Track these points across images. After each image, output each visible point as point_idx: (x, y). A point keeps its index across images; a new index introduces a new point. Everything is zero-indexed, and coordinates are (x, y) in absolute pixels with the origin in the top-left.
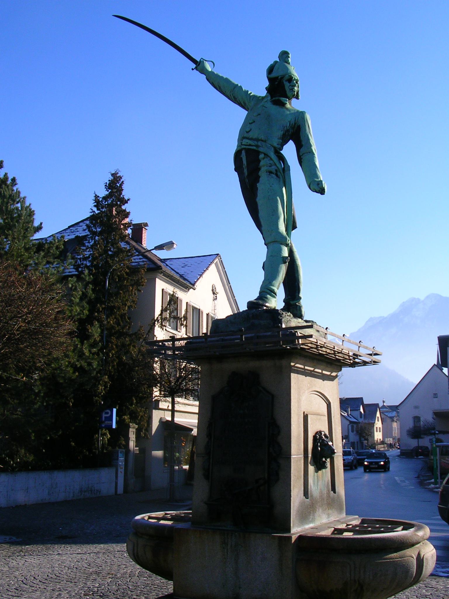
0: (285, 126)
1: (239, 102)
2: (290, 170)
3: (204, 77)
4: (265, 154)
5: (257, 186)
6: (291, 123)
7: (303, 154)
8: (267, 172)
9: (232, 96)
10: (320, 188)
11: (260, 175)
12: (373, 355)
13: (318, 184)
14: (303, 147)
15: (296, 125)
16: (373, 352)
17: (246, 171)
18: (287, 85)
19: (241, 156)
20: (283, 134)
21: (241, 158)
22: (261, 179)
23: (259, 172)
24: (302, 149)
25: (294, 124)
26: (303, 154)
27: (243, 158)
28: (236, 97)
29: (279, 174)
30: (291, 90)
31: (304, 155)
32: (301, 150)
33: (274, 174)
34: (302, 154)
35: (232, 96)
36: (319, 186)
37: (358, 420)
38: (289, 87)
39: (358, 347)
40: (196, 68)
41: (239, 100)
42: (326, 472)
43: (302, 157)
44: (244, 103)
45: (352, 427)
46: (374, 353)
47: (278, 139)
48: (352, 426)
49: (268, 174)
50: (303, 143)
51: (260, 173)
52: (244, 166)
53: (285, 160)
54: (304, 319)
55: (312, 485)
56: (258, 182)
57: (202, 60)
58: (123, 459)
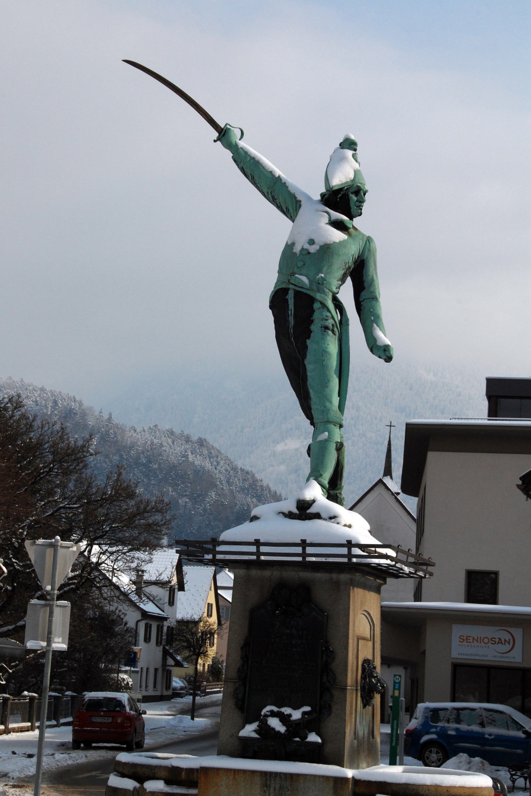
0: (347, 262)
1: (279, 205)
2: (349, 325)
3: (229, 154)
4: (321, 303)
5: (306, 342)
6: (354, 258)
7: (364, 300)
8: (321, 327)
9: (269, 193)
10: (387, 356)
11: (312, 329)
12: (418, 564)
13: (385, 350)
14: (365, 290)
15: (360, 258)
16: (418, 560)
17: (292, 320)
18: (354, 198)
19: (287, 297)
20: (344, 273)
21: (287, 301)
22: (312, 335)
23: (310, 325)
24: (363, 292)
25: (357, 257)
26: (364, 300)
27: (289, 300)
28: (276, 198)
29: (336, 329)
30: (358, 207)
31: (365, 301)
32: (363, 293)
33: (330, 330)
34: (362, 300)
35: (269, 193)
36: (387, 353)
37: (163, 611)
38: (355, 203)
39: (406, 556)
40: (219, 139)
41: (280, 203)
42: (370, 708)
43: (362, 303)
44: (287, 208)
45: (148, 628)
46: (420, 562)
47: (338, 281)
48: (146, 625)
49: (324, 329)
50: (366, 285)
51: (312, 327)
52: (290, 312)
53: (344, 311)
54: (343, 523)
55: (359, 726)
56: (309, 337)
57: (228, 126)
58: (45, 740)
